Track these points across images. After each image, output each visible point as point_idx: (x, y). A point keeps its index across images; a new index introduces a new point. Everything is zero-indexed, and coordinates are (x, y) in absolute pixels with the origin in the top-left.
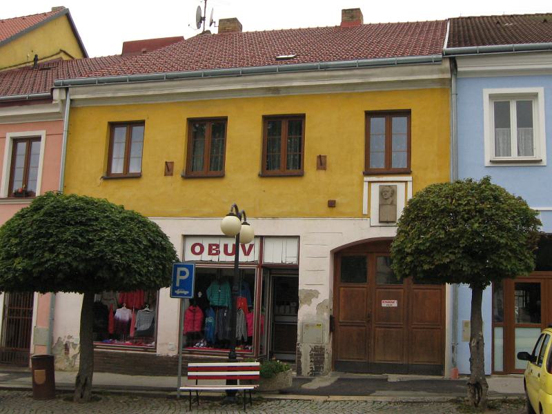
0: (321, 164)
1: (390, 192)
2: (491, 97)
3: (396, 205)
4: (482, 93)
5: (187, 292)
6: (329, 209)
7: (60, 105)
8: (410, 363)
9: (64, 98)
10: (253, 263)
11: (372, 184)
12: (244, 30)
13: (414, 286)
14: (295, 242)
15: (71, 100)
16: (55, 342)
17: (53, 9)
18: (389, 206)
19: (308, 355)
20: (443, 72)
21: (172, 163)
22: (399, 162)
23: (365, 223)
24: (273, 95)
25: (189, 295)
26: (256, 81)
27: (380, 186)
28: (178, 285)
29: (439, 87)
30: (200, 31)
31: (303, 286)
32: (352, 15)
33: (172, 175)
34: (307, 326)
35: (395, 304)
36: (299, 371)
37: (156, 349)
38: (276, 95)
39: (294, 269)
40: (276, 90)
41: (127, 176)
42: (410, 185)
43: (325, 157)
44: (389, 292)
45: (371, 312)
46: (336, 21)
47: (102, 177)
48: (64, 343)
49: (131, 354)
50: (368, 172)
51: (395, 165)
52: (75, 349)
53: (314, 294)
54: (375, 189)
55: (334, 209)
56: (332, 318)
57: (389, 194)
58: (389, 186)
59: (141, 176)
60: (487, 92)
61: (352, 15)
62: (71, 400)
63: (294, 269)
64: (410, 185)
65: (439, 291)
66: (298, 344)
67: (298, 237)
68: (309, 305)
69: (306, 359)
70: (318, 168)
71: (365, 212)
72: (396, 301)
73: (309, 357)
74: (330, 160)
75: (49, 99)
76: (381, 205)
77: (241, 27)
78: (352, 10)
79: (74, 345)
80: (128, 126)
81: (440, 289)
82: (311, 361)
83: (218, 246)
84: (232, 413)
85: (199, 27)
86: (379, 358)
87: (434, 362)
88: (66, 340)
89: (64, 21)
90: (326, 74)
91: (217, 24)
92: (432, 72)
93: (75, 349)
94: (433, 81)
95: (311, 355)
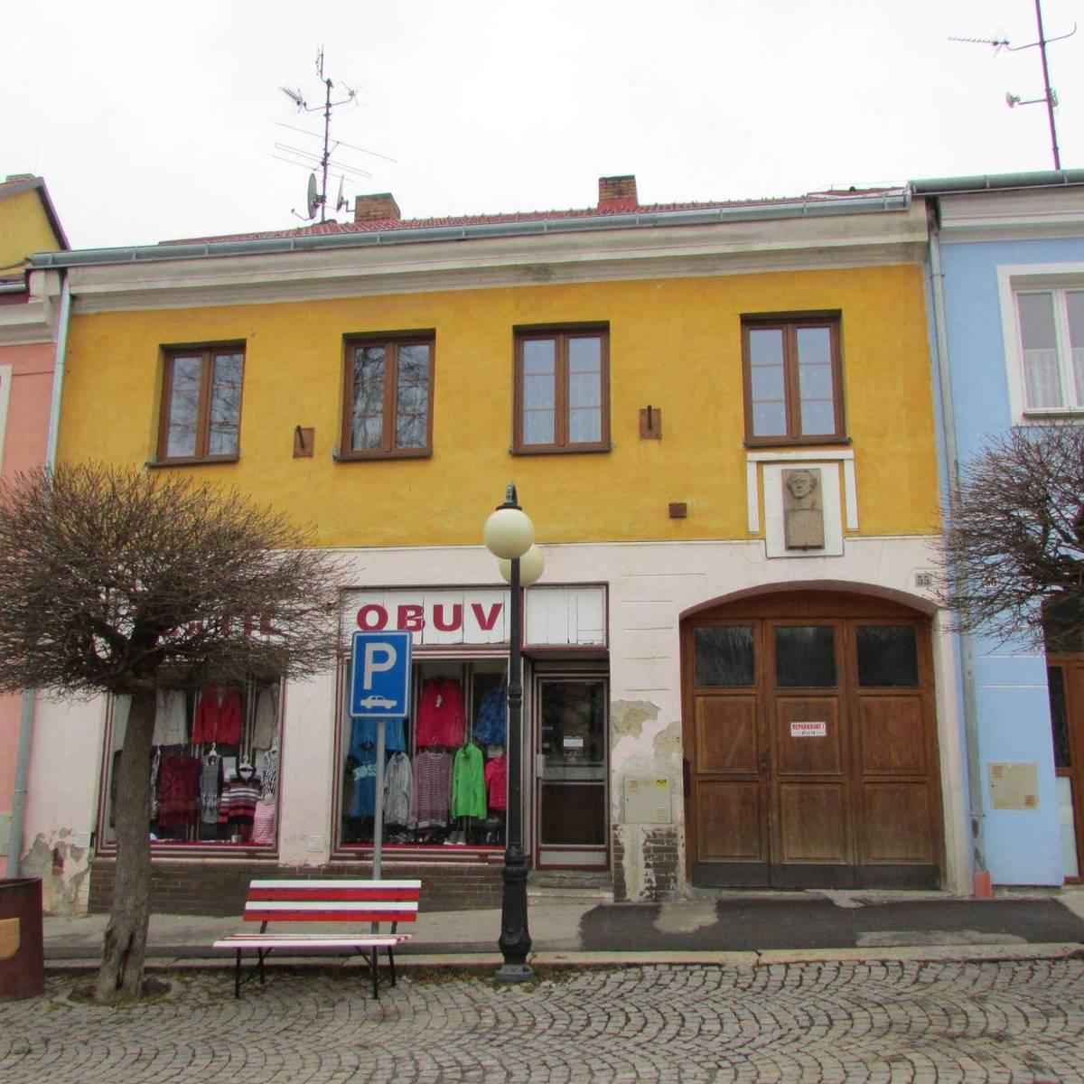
0: (650, 427)
1: (808, 484)
2: (1016, 282)
3: (821, 512)
4: (995, 273)
5: (394, 703)
6: (672, 523)
7: (47, 304)
8: (863, 863)
9: (55, 291)
10: (499, 646)
11: (766, 468)
12: (402, 218)
13: (860, 691)
14: (598, 595)
15: (73, 297)
16: (30, 844)
17: (10, 178)
18: (807, 513)
19: (641, 851)
20: (910, 228)
21: (311, 430)
22: (818, 420)
23: (755, 549)
24: (535, 284)
25: (399, 709)
26: (500, 252)
27: (784, 472)
28: (368, 685)
29: (900, 263)
30: (318, 220)
31: (619, 692)
32: (618, 190)
33: (310, 455)
34: (634, 783)
35: (819, 730)
36: (620, 889)
37: (276, 850)
38: (542, 283)
39: (596, 660)
40: (543, 271)
41: (203, 460)
42: (849, 468)
43: (658, 411)
44: (806, 703)
45: (769, 750)
46: (589, 198)
47: (146, 464)
48: (52, 848)
49: (216, 865)
50: (753, 444)
51: (809, 428)
52: (77, 858)
53: (642, 712)
54: (774, 477)
55: (683, 522)
56: (686, 763)
57: (806, 489)
58: (806, 471)
59: (238, 458)
60: (1005, 272)
61: (618, 190)
62: (87, 996)
63: (596, 660)
64: (849, 468)
65: (916, 699)
66: (615, 827)
67: (606, 585)
68: (637, 737)
69: (635, 862)
70: (643, 436)
71: (754, 526)
72: (823, 724)
73: (641, 856)
74: (668, 421)
75: (23, 295)
76: (788, 514)
77: (399, 216)
78: (619, 179)
79: (77, 852)
80: (207, 355)
81: (918, 696)
82: (647, 866)
83: (419, 610)
84: (976, 1071)
85: (312, 217)
86: (793, 853)
87: (918, 859)
88: (57, 839)
89: (33, 201)
90: (656, 233)
91: (352, 206)
92: (888, 229)
93: (77, 858)
94: (887, 248)
95: (647, 851)
